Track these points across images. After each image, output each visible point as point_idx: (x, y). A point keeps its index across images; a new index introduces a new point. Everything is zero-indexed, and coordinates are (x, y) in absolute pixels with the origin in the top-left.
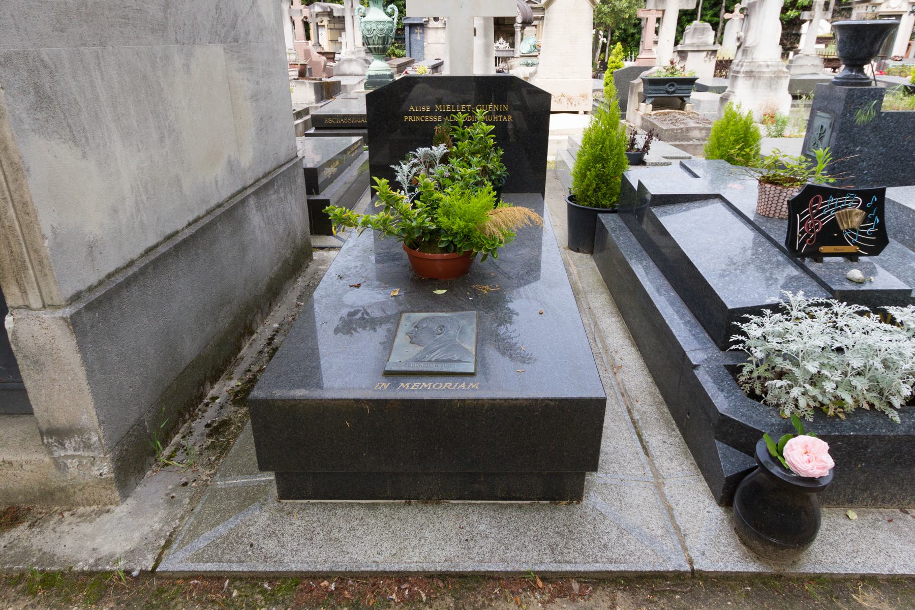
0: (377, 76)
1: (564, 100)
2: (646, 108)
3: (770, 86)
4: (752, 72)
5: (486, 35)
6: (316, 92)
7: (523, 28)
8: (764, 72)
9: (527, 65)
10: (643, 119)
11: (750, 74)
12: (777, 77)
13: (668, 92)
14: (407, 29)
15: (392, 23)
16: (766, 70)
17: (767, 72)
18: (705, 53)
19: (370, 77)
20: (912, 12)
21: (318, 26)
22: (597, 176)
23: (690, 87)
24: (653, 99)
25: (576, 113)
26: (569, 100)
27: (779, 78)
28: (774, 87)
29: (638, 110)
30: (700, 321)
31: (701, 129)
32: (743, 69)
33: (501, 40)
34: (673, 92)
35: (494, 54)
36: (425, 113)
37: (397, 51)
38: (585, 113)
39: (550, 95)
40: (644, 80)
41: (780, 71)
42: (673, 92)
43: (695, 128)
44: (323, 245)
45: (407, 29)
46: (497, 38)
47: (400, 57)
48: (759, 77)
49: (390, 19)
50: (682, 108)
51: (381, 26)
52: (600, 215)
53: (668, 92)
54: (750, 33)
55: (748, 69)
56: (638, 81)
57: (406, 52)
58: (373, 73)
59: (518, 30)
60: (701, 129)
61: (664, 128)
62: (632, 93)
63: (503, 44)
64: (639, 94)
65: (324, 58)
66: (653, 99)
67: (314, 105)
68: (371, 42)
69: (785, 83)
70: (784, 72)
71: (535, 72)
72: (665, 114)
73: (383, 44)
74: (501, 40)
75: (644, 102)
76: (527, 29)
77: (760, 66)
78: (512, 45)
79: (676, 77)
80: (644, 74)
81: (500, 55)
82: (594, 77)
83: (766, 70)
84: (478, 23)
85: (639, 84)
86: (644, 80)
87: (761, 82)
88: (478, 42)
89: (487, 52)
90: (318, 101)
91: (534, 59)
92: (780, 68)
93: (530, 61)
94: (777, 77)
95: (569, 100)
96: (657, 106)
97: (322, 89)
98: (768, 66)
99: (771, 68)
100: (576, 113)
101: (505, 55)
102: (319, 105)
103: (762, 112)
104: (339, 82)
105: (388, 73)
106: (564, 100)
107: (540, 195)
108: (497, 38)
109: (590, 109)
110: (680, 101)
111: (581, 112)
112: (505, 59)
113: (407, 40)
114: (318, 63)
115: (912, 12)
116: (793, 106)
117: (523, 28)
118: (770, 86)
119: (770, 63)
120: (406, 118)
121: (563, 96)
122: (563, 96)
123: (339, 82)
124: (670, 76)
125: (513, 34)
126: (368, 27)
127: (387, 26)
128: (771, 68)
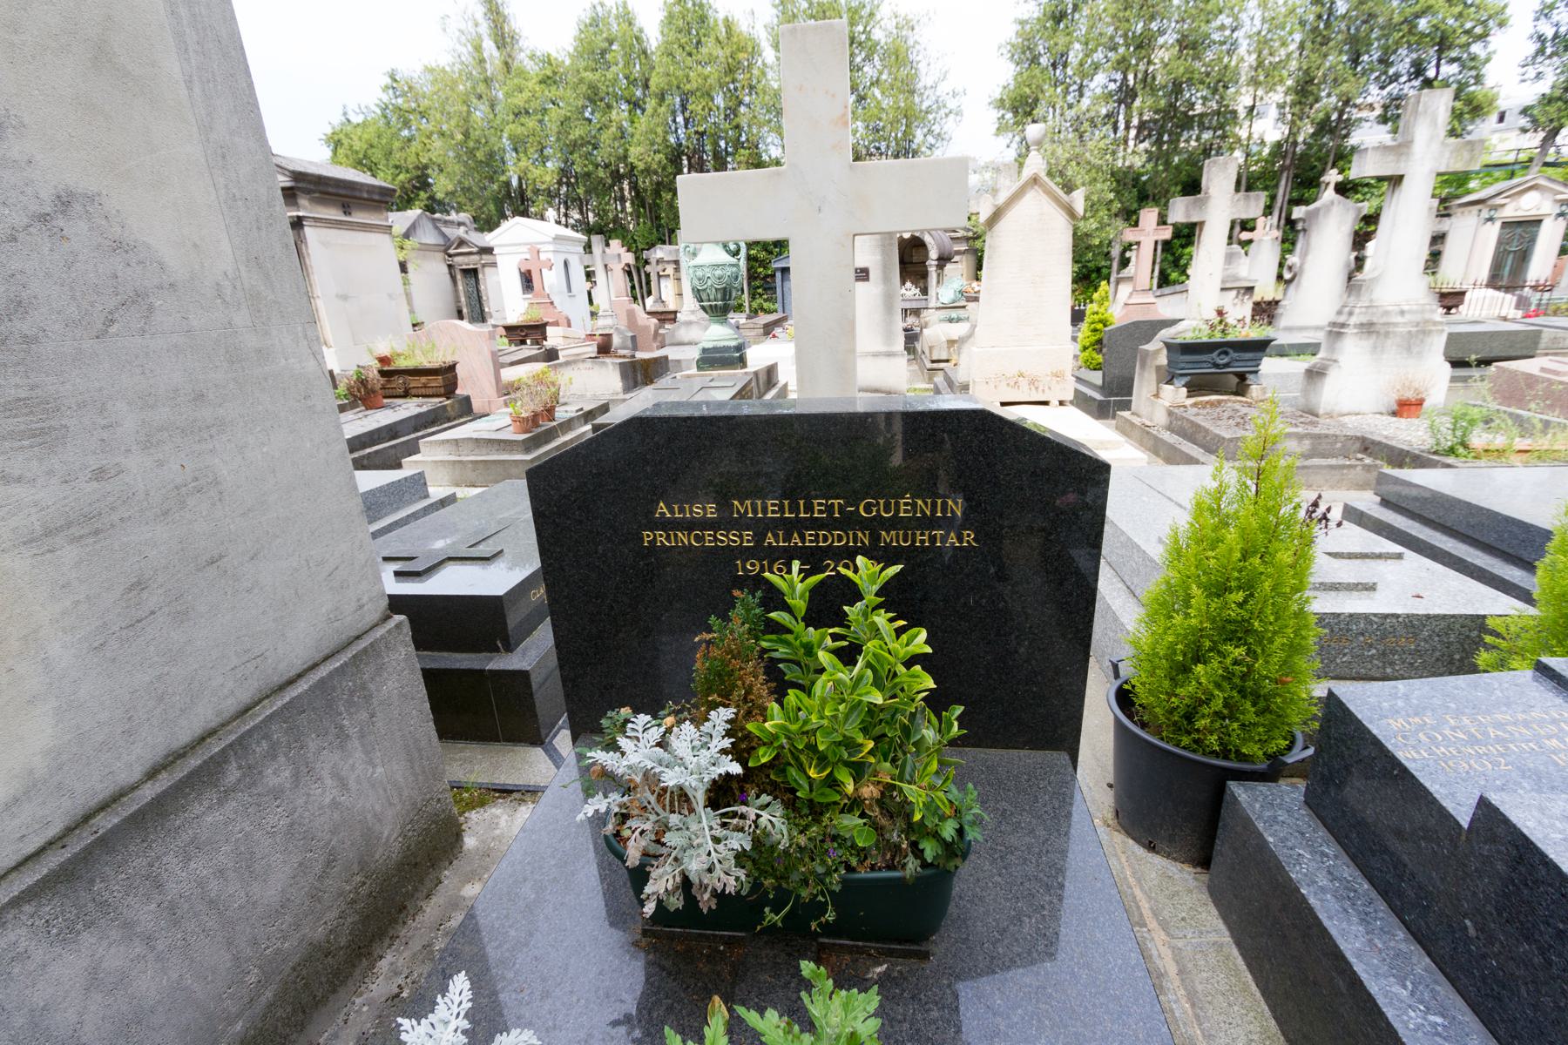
0: (715, 349)
1: (1023, 382)
2: (1175, 394)
3: (1409, 349)
4: (1371, 324)
5: (886, 279)
6: (624, 376)
7: (941, 267)
8: (1396, 325)
9: (951, 320)
10: (1170, 413)
11: (1368, 328)
12: (1422, 331)
13: (1216, 366)
14: (779, 275)
15: (736, 265)
16: (1399, 319)
17: (1403, 324)
18: (1234, 293)
19: (704, 350)
20: (1561, 214)
21: (659, 276)
22: (1228, 676)
23: (1258, 354)
24: (1187, 379)
25: (1045, 403)
26: (1032, 382)
27: (1425, 333)
28: (1415, 350)
29: (1157, 395)
30: (1412, 934)
31: (1300, 437)
32: (1353, 320)
33: (908, 284)
34: (1227, 365)
35: (900, 305)
36: (705, 524)
37: (766, 305)
38: (1061, 403)
39: (1104, 468)
40: (1168, 346)
41: (1426, 322)
42: (1227, 365)
43: (1289, 435)
44: (504, 779)
45: (779, 275)
46: (903, 283)
47: (770, 312)
48: (1387, 334)
49: (733, 260)
50: (1241, 388)
51: (718, 272)
52: (1234, 787)
53: (1216, 366)
54: (1310, 257)
55: (1364, 319)
56: (1155, 345)
57: (778, 306)
58: (710, 345)
59: (932, 270)
60: (1300, 437)
61: (1227, 436)
62: (1143, 366)
63: (911, 290)
64: (1158, 368)
65: (654, 321)
66: (1187, 379)
67: (621, 396)
68: (704, 296)
69: (1439, 343)
70: (1435, 323)
71: (971, 335)
72: (1212, 404)
73: (724, 299)
74: (908, 284)
75: (1170, 382)
76: (949, 266)
77: (1387, 313)
78: (925, 291)
79: (1229, 338)
80: (1165, 334)
81: (908, 305)
82: (781, 245)
83: (1399, 319)
84: (867, 254)
85: (1157, 352)
86: (1168, 346)
87: (1389, 342)
88: (867, 296)
89: (888, 300)
90: (627, 389)
91: (961, 312)
92: (1427, 316)
93: (954, 314)
94: (1422, 331)
95: (1032, 382)
96: (1195, 388)
97: (635, 371)
98: (1402, 313)
99: (1408, 318)
100: (1045, 403)
101: (914, 305)
102: (628, 396)
103: (1395, 397)
104: (666, 358)
105: (733, 343)
106: (1023, 382)
107: (1064, 757)
108: (903, 283)
109: (1070, 396)
110: (1235, 380)
111: (1055, 402)
112: (916, 312)
113: (779, 290)
114: (647, 328)
115: (1561, 214)
116: (1453, 379)
117: (941, 267)
118: (1409, 349)
119: (1406, 308)
120: (648, 536)
121: (1021, 375)
122: (1021, 375)
123: (666, 358)
124: (1218, 338)
125: (924, 275)
126: (700, 273)
127: (729, 271)
128: (1408, 318)
